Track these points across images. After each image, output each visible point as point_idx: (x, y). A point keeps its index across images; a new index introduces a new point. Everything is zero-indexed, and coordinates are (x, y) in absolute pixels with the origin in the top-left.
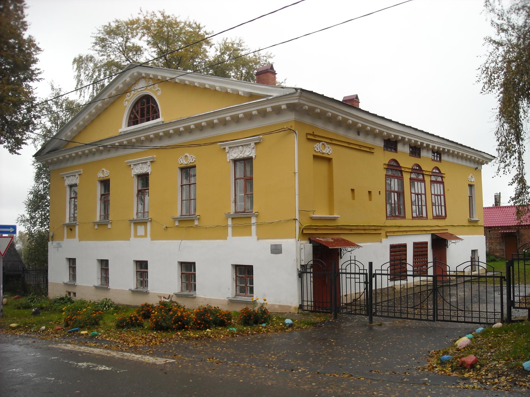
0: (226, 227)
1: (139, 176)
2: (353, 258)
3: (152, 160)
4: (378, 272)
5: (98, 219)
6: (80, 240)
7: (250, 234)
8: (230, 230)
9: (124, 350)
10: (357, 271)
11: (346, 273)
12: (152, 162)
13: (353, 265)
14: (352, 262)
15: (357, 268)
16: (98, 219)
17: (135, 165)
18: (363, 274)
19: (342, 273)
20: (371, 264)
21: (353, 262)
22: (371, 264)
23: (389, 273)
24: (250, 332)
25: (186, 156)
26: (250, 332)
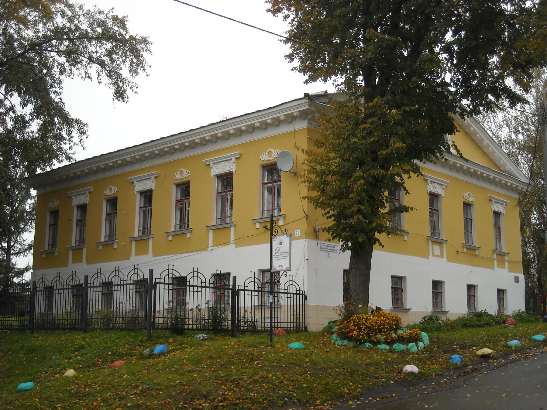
0: (493, 259)
1: (142, 193)
2: (171, 267)
3: (156, 176)
4: (158, 281)
5: (136, 235)
6: (155, 255)
7: (504, 268)
8: (495, 262)
9: (109, 342)
10: (199, 284)
11: (164, 283)
12: (155, 177)
13: (195, 278)
14: (195, 274)
15: (199, 281)
16: (136, 235)
17: (495, 202)
18: (302, 294)
19: (168, 284)
20: (151, 272)
21: (195, 274)
22: (151, 272)
23: (269, 290)
24: (375, 355)
25: (182, 171)
26: (375, 355)
